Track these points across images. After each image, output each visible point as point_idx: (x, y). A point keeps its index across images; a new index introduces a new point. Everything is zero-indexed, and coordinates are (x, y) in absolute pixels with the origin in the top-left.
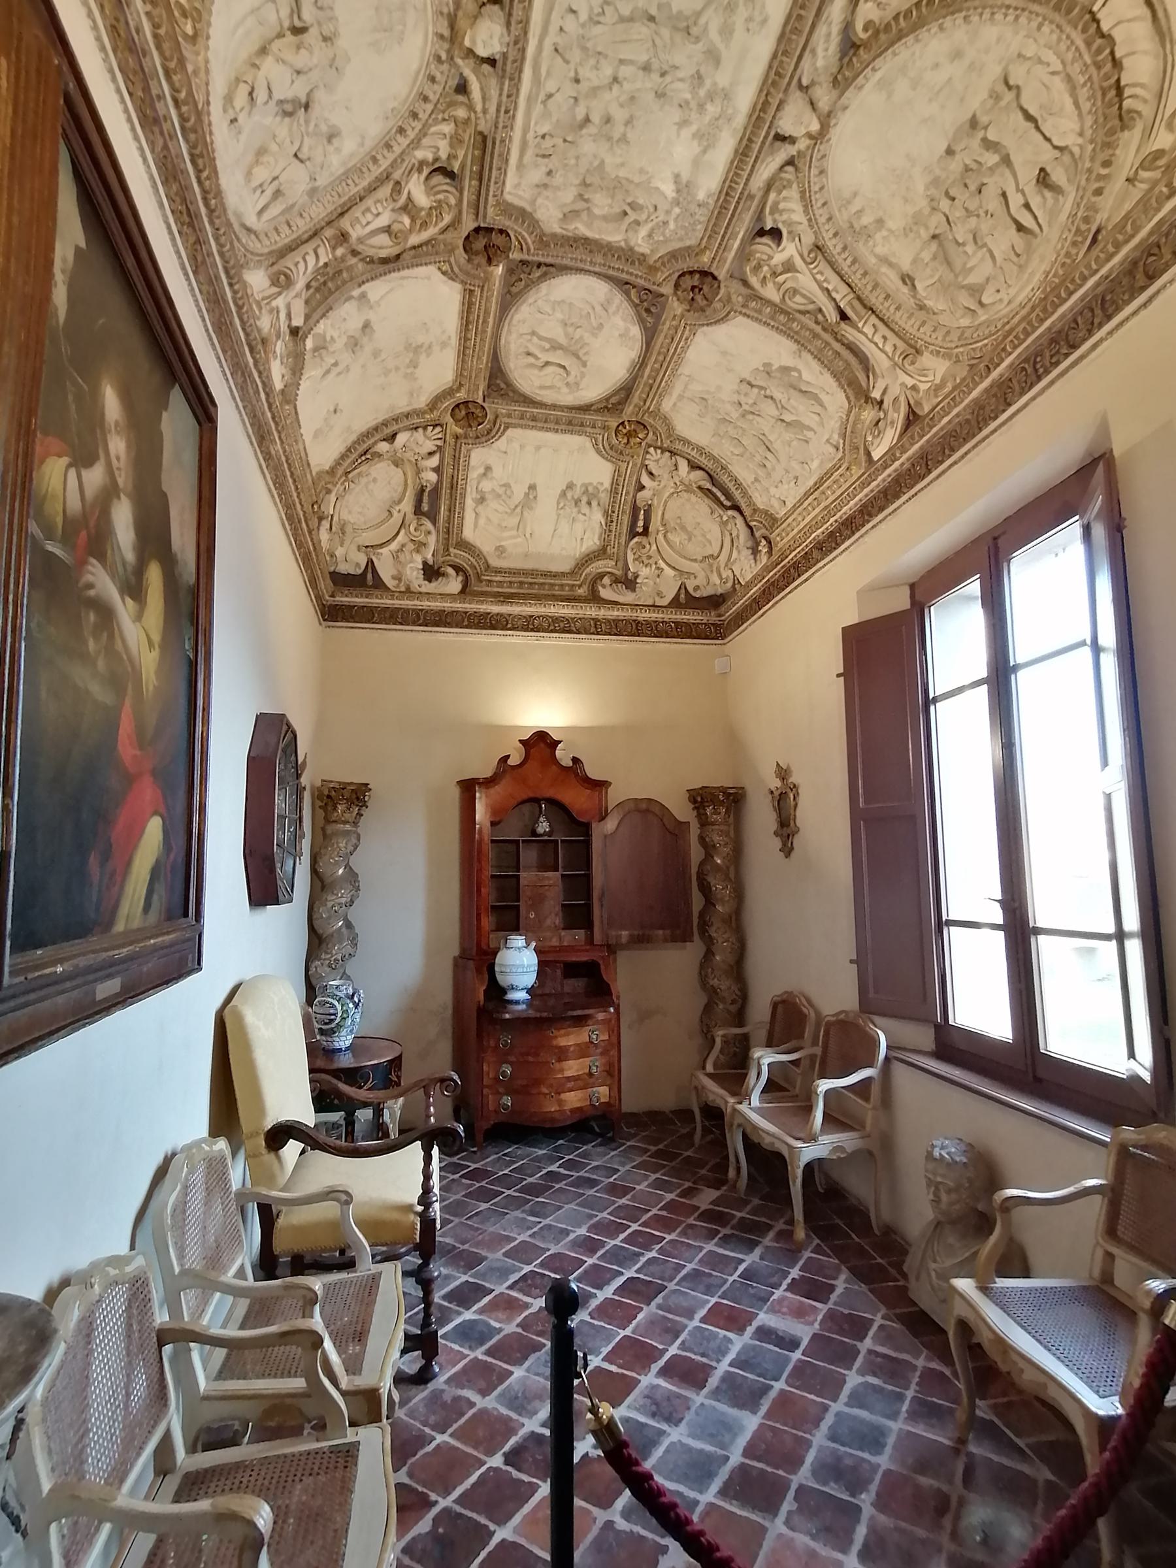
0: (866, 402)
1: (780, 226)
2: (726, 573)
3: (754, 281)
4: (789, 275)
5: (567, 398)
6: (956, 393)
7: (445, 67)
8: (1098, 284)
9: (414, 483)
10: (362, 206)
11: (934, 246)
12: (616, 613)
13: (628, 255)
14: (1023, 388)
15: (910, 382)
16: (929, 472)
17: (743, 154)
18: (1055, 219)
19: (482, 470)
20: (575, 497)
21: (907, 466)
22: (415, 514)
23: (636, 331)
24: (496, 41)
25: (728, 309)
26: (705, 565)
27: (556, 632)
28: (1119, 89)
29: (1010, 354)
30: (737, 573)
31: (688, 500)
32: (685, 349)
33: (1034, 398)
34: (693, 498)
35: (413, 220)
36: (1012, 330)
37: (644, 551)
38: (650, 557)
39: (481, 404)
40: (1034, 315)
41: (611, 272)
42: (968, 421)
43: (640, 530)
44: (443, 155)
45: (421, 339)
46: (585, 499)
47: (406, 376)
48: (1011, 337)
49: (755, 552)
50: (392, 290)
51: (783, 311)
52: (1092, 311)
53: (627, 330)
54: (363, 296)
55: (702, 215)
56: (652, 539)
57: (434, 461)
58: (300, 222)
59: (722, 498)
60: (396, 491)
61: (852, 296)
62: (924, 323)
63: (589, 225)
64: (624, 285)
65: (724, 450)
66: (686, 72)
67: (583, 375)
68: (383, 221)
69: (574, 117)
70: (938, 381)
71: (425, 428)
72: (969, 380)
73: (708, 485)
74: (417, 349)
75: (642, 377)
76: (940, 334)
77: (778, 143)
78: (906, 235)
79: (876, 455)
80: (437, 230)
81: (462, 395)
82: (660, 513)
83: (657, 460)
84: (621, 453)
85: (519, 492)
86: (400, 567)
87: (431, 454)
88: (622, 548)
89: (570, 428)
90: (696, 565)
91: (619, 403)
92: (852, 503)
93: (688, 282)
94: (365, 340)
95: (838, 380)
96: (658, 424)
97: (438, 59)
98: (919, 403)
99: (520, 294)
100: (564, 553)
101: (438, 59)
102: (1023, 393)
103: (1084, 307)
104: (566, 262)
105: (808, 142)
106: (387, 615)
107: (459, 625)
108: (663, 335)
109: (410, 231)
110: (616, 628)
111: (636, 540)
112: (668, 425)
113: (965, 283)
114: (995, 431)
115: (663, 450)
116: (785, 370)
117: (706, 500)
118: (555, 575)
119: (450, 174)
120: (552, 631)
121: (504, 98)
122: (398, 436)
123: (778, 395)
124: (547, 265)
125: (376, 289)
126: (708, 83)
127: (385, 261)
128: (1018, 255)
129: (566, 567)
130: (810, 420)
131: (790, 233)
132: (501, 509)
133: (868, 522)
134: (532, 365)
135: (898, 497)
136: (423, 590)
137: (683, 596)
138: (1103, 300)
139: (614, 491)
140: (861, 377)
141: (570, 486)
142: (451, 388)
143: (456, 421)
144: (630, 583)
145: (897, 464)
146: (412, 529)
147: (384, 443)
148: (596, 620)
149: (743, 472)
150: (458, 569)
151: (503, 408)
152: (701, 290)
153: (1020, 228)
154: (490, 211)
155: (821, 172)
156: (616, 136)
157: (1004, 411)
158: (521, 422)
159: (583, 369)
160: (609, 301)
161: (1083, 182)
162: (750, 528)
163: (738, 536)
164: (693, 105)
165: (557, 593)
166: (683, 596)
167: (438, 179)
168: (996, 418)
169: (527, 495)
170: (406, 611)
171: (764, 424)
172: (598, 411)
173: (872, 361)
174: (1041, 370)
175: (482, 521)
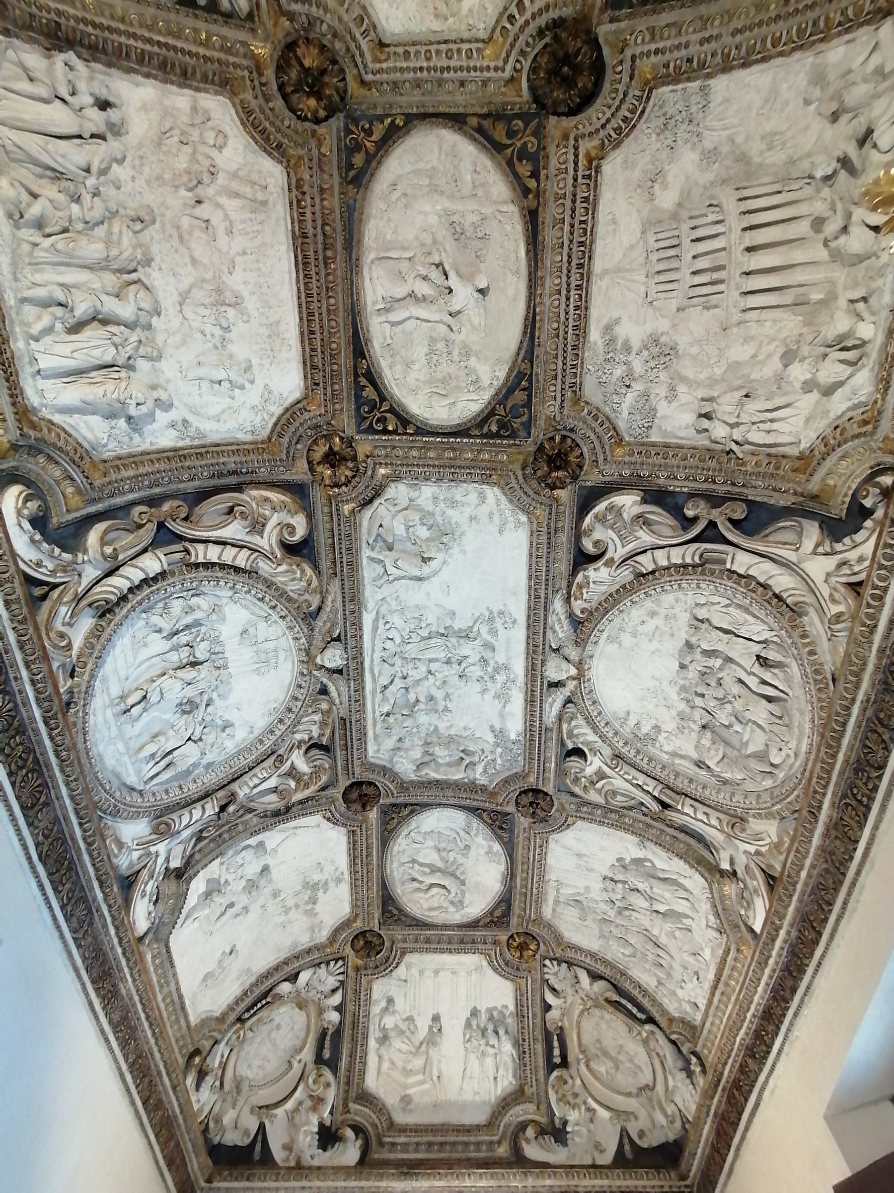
0: (722, 876)
1: (580, 746)
2: (670, 1109)
3: (577, 790)
4: (604, 781)
5: (456, 917)
6: (796, 844)
7: (308, 678)
8: (864, 710)
9: (316, 1025)
10: (251, 773)
11: (708, 734)
13: (472, 787)
14: (858, 822)
15: (752, 849)
16: (820, 934)
17: (532, 702)
18: (793, 680)
19: (383, 1004)
20: (482, 1026)
21: (794, 934)
23: (497, 847)
24: (337, 658)
25: (564, 815)
26: (643, 1099)
28: (777, 597)
29: (824, 794)
31: (602, 1018)
32: (543, 855)
33: (876, 827)
35: (298, 782)
36: (812, 773)
37: (567, 1087)
38: (576, 1095)
39: (378, 935)
40: (822, 754)
41: (463, 803)
42: (827, 871)
43: (557, 1060)
44: (315, 734)
45: (316, 877)
46: (491, 1027)
47: (306, 912)
48: (815, 780)
49: (690, 1074)
51: (612, 811)
52: (876, 732)
53: (490, 847)
54: (261, 844)
55: (518, 749)
57: (337, 999)
58: (192, 787)
59: (635, 1011)
60: (298, 1037)
61: (661, 786)
62: (733, 794)
63: (437, 771)
64: (473, 810)
65: (616, 953)
66: (474, 658)
67: (463, 893)
68: (272, 783)
69: (408, 701)
70: (775, 840)
71: (328, 963)
72: (801, 829)
73: (616, 997)
76: (752, 799)
77: (552, 689)
78: (683, 733)
79: (758, 928)
80: (316, 787)
81: (358, 925)
83: (555, 974)
84: (518, 969)
85: (423, 1025)
87: (334, 991)
88: (542, 1086)
91: (503, 916)
92: (760, 989)
93: (525, 800)
94: (263, 882)
95: (685, 861)
96: (544, 933)
97: (302, 674)
98: (770, 866)
100: (477, 1098)
101: (302, 674)
102: (861, 826)
103: (865, 733)
104: (425, 800)
105: (575, 682)
109: (296, 791)
111: (555, 1073)
113: (748, 752)
114: (858, 873)
115: (560, 961)
116: (638, 862)
118: (468, 1130)
119: (326, 749)
121: (352, 693)
122: (301, 975)
123: (641, 886)
124: (411, 805)
125: (272, 838)
126: (492, 663)
127: (277, 814)
128: (780, 718)
129: (480, 1117)
130: (682, 907)
131: (590, 750)
132: (404, 1047)
133: (787, 1009)
134: (418, 889)
135: (804, 972)
136: (316, 1163)
137: (627, 1148)
138: (878, 719)
139: (520, 1015)
140: (706, 853)
141: (475, 1013)
142: (349, 920)
143: (357, 951)
144: (557, 1133)
145: (782, 933)
146: (311, 1081)
147: (286, 984)
149: (643, 975)
150: (358, 1130)
151: (399, 933)
152: (538, 804)
153: (769, 699)
154: (357, 770)
155: (594, 703)
156: (441, 708)
157: (855, 849)
158: (415, 945)
160: (469, 826)
161: (796, 652)
164: (486, 678)
165: (473, 1155)
166: (627, 1148)
167: (315, 752)
168: (851, 858)
169: (430, 1027)
171: (644, 920)
172: (486, 926)
173: (708, 838)
174: (865, 800)
175: (386, 1066)
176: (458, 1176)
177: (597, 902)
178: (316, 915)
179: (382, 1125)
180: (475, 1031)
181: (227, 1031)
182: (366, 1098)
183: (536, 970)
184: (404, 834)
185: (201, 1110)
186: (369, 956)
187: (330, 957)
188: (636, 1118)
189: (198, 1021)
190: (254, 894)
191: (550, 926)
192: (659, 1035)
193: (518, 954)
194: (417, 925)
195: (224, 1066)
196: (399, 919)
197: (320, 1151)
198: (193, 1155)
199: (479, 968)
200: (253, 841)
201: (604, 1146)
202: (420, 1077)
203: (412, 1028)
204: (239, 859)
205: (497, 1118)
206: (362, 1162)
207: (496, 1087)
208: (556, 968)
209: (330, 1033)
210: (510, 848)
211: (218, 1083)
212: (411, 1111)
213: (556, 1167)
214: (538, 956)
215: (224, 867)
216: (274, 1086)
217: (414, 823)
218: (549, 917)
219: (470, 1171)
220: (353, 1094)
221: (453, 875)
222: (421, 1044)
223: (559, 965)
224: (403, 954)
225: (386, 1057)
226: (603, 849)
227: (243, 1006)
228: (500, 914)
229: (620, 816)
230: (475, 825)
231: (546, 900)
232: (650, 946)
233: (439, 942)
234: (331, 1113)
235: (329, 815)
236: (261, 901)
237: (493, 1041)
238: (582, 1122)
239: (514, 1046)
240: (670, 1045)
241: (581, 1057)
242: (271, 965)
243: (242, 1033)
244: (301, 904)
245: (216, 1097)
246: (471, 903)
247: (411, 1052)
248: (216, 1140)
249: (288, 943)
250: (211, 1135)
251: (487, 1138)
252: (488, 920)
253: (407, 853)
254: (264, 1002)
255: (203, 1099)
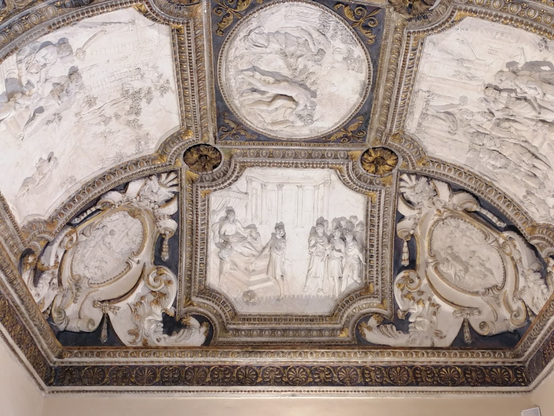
5: (304, 131)
9: (152, 231)
12: (387, 359)
19: (223, 214)
22: (155, 263)
23: (359, 51)
25: (450, 9)
27: (316, 384)
30: (529, 303)
31: (457, 227)
32: (415, 61)
34: (463, 225)
37: (413, 286)
38: (421, 293)
39: (214, 146)
43: (406, 263)
45: (137, 85)
46: (338, 234)
47: (129, 123)
50: (94, 36)
53: (350, 51)
54: (63, 42)
56: (421, 272)
57: (172, 208)
59: (495, 220)
65: (485, 165)
67: (314, 105)
71: (159, 176)
73: (475, 208)
74: (136, 95)
75: (377, 98)
81: (191, 138)
82: (426, 244)
83: (411, 187)
84: (371, 183)
85: (266, 233)
86: (138, 321)
87: (168, 201)
88: (388, 285)
89: (310, 161)
90: (478, 299)
94: (72, 86)
96: (405, 147)
99: (353, 118)
100: (321, 294)
106: (120, 375)
107: (201, 382)
108: (388, 50)
110: (388, 377)
111: (402, 274)
112: (417, 147)
115: (418, 176)
116: (533, 66)
117: (476, 223)
118: (312, 319)
120: (310, 384)
123: (531, 93)
129: (325, 309)
132: (246, 251)
134: (260, 102)
136: (162, 344)
137: (467, 335)
139: (370, 222)
141: (321, 222)
142: (179, 133)
143: (190, 165)
144: (401, 323)
146: (151, 279)
148: (363, 369)
150: (202, 319)
151: (237, 148)
159: (313, 99)
162: (532, 247)
163: (520, 260)
165: (316, 339)
166: (467, 335)
170: (142, 369)
171: (525, 131)
175: (227, 267)
176: (300, 354)
177: (472, 114)
178: (140, 126)
179: (226, 315)
180: (321, 238)
181: (58, 233)
182: (209, 293)
183: (391, 184)
184: (242, 34)
185: (42, 303)
186: (204, 169)
187: (161, 169)
188: (480, 312)
189: (25, 223)
190: (65, 99)
191: (412, 141)
192: (518, 241)
193: (373, 169)
194: (258, 140)
195: (60, 266)
196: (239, 134)
197: (166, 336)
198: (41, 337)
199: (327, 183)
200: (53, 37)
201: (445, 333)
202: (264, 276)
203: (254, 234)
204: (39, 57)
205: (340, 310)
206: (207, 343)
207: (340, 285)
208: (414, 182)
209: (167, 238)
210: (374, 52)
211: (55, 281)
212: (254, 304)
213: (395, 348)
214: (395, 171)
215: (23, 66)
216: (111, 285)
217: (254, 20)
218: (413, 131)
219: (313, 350)
220: (196, 288)
221: (302, 85)
222: (264, 248)
223: (417, 179)
224: (243, 167)
225: (227, 259)
226: (492, 52)
227: (71, 211)
228: (355, 128)
229: (524, 9)
230: (332, 24)
231: (412, 113)
232: (527, 158)
233: (283, 157)
234: (174, 305)
235: (145, 7)
236: (74, 109)
237: (340, 245)
238: (425, 314)
239: (361, 251)
240: (528, 249)
241: (430, 260)
242: (96, 174)
243: (74, 236)
244: (122, 114)
245: (56, 292)
246: (322, 116)
247: (254, 256)
248: (62, 327)
249: (112, 155)
250: (57, 322)
251: (329, 326)
252: (341, 134)
253: (246, 58)
254: (93, 209)
255: (43, 292)
